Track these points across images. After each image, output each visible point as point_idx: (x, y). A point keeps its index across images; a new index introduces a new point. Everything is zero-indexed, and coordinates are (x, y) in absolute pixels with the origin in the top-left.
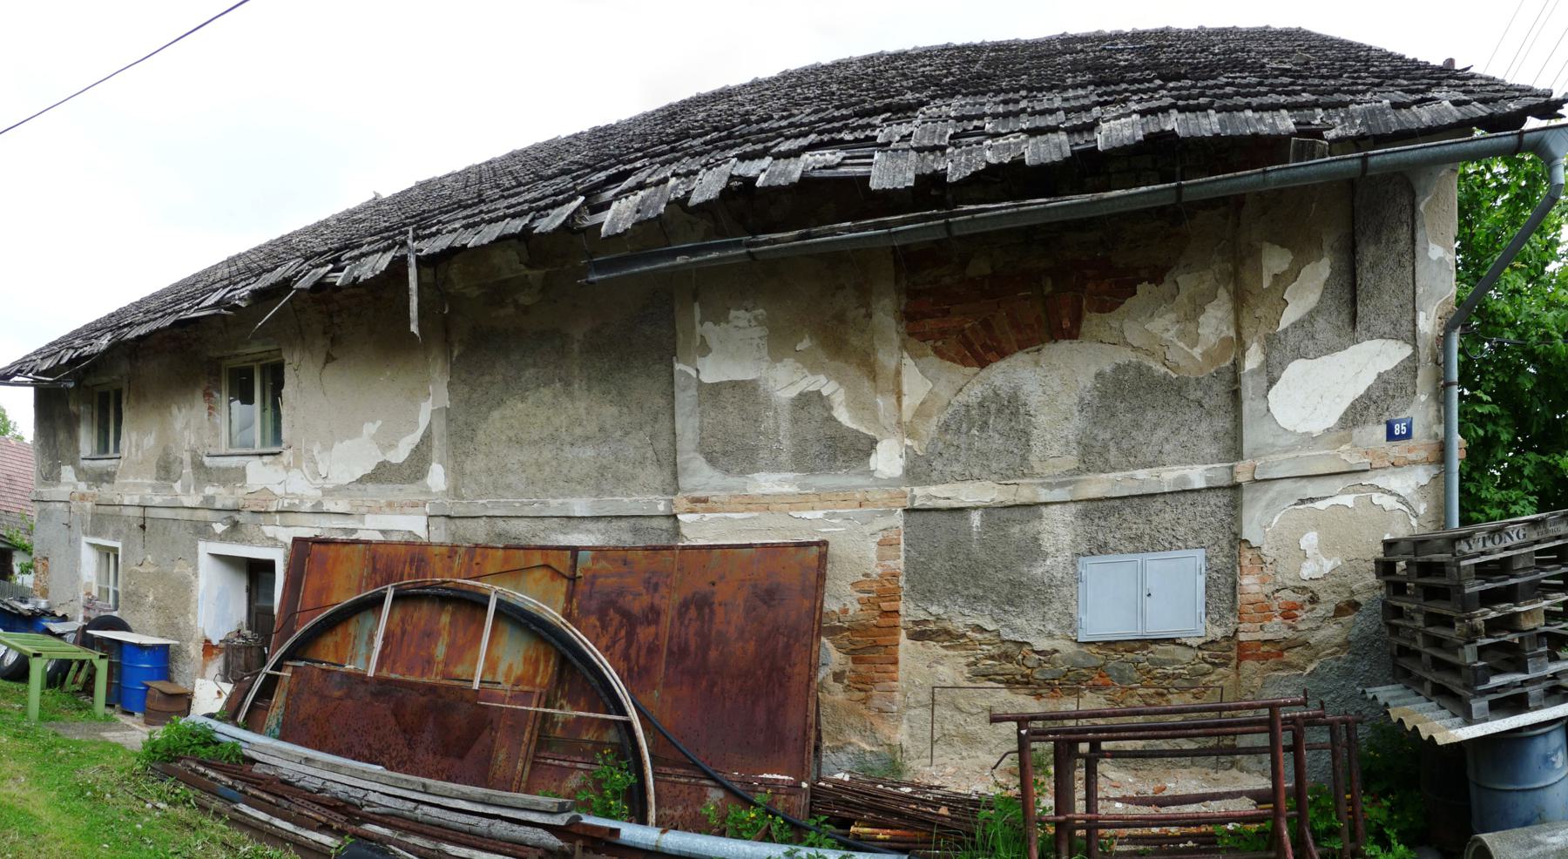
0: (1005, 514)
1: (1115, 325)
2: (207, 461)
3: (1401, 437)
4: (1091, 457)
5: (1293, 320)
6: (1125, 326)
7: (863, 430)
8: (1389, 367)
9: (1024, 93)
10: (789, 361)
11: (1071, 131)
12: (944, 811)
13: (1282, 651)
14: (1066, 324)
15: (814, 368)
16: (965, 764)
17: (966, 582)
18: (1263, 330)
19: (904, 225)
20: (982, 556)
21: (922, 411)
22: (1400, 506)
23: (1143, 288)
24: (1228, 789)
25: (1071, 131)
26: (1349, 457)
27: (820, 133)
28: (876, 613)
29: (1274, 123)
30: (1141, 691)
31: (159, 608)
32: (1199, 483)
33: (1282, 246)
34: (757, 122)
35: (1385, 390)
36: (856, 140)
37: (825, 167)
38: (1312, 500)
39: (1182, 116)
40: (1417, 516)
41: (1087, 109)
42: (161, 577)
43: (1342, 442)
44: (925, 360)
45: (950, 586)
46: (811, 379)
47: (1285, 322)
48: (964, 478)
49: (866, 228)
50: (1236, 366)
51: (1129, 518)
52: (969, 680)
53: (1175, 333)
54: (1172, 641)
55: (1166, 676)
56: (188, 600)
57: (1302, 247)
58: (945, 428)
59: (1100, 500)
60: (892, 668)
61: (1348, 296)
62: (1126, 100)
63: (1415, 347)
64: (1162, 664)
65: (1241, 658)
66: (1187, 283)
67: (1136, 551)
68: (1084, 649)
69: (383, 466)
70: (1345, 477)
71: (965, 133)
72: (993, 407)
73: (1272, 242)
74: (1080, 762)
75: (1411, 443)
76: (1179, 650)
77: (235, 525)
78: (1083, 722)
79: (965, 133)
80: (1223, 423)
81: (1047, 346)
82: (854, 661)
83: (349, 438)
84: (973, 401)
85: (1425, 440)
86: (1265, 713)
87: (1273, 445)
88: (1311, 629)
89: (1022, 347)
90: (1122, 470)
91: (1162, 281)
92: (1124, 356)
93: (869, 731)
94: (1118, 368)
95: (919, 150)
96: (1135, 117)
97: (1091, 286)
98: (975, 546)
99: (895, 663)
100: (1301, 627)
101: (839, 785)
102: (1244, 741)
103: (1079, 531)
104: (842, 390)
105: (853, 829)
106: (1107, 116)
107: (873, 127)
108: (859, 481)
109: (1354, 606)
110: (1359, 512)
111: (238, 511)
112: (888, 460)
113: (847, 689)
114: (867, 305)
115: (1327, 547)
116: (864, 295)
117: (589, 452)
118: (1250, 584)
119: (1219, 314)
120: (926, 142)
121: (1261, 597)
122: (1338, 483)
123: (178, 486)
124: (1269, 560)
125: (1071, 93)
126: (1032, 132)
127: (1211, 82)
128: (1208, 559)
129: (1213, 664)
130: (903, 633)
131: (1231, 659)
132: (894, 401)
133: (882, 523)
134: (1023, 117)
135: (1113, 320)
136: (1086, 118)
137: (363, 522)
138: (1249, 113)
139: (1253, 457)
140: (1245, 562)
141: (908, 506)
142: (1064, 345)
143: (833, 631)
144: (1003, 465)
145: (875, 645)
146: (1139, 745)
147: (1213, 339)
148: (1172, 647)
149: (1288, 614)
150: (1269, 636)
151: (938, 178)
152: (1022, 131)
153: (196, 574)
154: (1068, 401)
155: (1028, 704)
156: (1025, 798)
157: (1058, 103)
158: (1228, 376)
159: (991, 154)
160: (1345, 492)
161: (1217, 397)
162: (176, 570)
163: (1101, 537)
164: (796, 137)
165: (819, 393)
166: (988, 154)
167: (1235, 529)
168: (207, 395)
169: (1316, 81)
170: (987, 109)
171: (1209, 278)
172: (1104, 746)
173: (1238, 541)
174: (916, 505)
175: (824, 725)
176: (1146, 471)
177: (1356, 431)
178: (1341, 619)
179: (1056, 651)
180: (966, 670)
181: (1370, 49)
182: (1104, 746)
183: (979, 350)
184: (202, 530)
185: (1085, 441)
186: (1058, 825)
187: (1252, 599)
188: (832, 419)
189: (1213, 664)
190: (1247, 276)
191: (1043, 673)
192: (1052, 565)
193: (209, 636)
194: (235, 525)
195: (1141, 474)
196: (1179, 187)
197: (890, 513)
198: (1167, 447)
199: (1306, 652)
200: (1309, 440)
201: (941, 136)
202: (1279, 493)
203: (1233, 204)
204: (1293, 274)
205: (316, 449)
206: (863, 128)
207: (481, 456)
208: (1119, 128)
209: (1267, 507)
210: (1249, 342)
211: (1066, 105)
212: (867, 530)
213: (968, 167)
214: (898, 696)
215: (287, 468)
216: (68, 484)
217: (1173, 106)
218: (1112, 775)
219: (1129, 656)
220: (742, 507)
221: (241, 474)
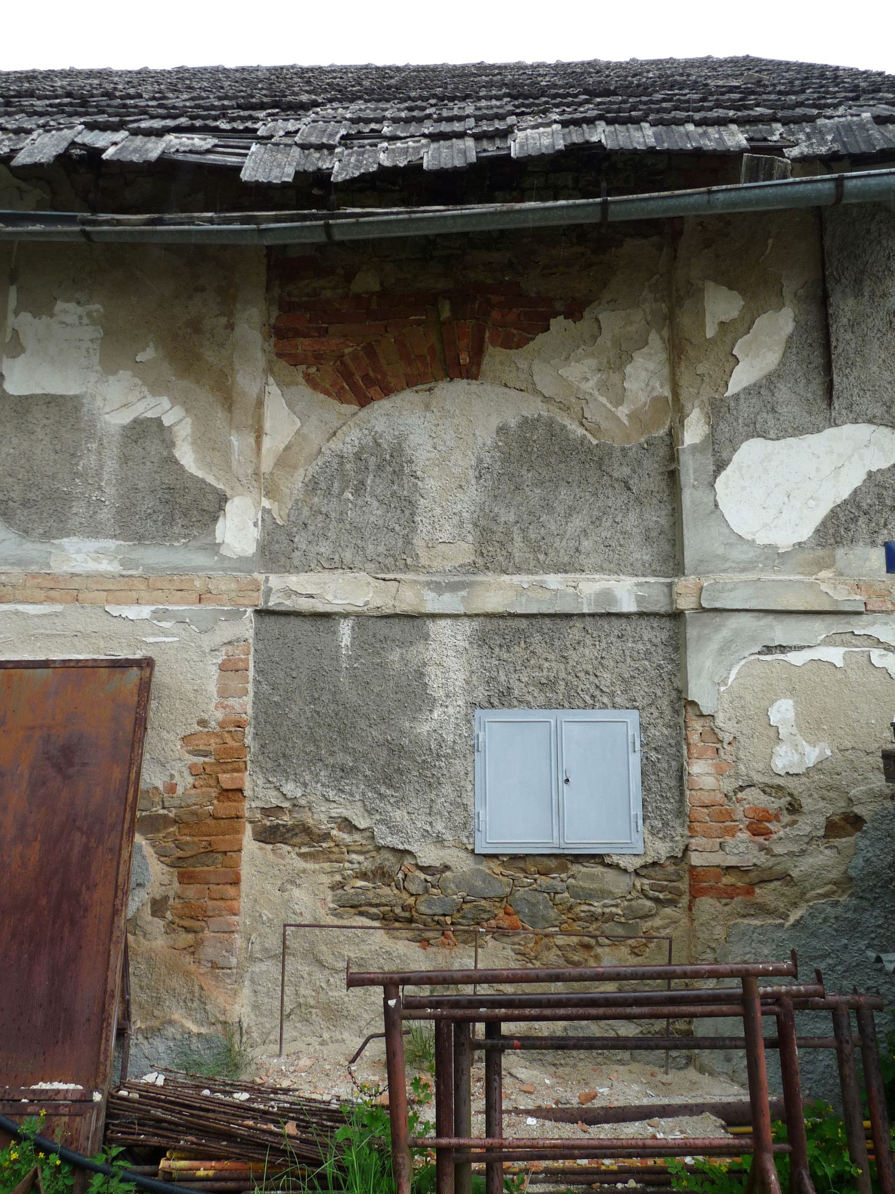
0: (382, 628)
1: (523, 365)
4: (492, 549)
5: (745, 383)
6: (535, 369)
7: (211, 480)
9: (433, 101)
10: (125, 375)
11: (478, 137)
12: (291, 1128)
13: (752, 885)
14: (464, 359)
15: (156, 388)
16: (319, 1057)
17: (332, 742)
18: (707, 392)
19: (275, 223)
20: (353, 697)
21: (284, 461)
23: (558, 324)
24: (679, 1104)
25: (478, 137)
26: (831, 590)
27: (192, 118)
28: (214, 792)
29: (721, 138)
30: (561, 940)
32: (628, 606)
33: (731, 288)
34: (121, 98)
35: (880, 497)
36: (234, 130)
37: (191, 152)
38: (782, 649)
39: (611, 128)
41: (502, 117)
43: (821, 565)
44: (293, 389)
45: (311, 748)
46: (151, 400)
48: (335, 565)
49: (229, 221)
50: (673, 438)
51: (539, 651)
52: (334, 913)
53: (595, 381)
55: (593, 917)
57: (757, 288)
58: (312, 486)
59: (501, 616)
60: (231, 891)
61: (818, 361)
62: (545, 112)
64: (587, 896)
65: (696, 892)
66: (612, 321)
67: (548, 706)
68: (484, 867)
70: (829, 619)
71: (360, 135)
72: (372, 461)
74: (480, 1054)
76: (610, 874)
78: (484, 990)
79: (360, 135)
80: (657, 517)
81: (441, 384)
82: (185, 878)
84: (349, 450)
86: (733, 985)
87: (725, 559)
88: (791, 854)
89: (411, 383)
90: (529, 572)
91: (581, 317)
92: (534, 408)
93: (197, 1001)
94: (525, 422)
95: (304, 147)
96: (555, 127)
97: (495, 314)
98: (344, 680)
99: (236, 882)
100: (778, 849)
101: (149, 1094)
102: (704, 1028)
103: (476, 664)
104: (189, 420)
105: (163, 1163)
106: (524, 125)
107: (256, 120)
108: (200, 559)
109: (854, 822)
112: (238, 530)
113: (170, 928)
114: (230, 314)
115: (810, 725)
116: (228, 300)
118: (700, 770)
119: (651, 366)
120: (313, 140)
121: (719, 797)
122: (819, 628)
124: (727, 738)
125: (483, 103)
126: (434, 137)
127: (644, 99)
128: (643, 728)
129: (656, 900)
130: (248, 827)
131: (680, 894)
132: (252, 441)
133: (226, 631)
134: (427, 123)
135: (521, 358)
136: (499, 125)
138: (691, 127)
139: (699, 574)
140: (694, 738)
142: (461, 385)
143: (154, 824)
144: (381, 549)
145: (210, 851)
146: (557, 1028)
147: (643, 398)
148: (599, 870)
149: (759, 827)
150: (732, 861)
151: (322, 177)
152: (424, 135)
154: (463, 462)
155: (408, 955)
156: (394, 1109)
157: (470, 109)
158: (663, 451)
159: (384, 157)
160: (829, 641)
161: (649, 480)
163: (502, 678)
164: (164, 118)
165: (158, 421)
166: (382, 156)
167: (677, 683)
169: (773, 97)
170: (388, 114)
171: (638, 317)
172: (506, 1028)
173: (682, 704)
174: (272, 604)
175: (136, 994)
176: (560, 576)
177: (840, 552)
178: (836, 842)
179: (447, 868)
180: (329, 896)
181: (837, 69)
182: (506, 1028)
183: (360, 383)
185: (482, 522)
186: (442, 1151)
187: (706, 799)
188: (172, 460)
189: (656, 900)
190: (686, 320)
191: (430, 903)
192: (438, 722)
195: (554, 580)
196: (605, 204)
197: (235, 615)
198: (586, 544)
199: (786, 890)
200: (772, 556)
201: (332, 135)
202: (736, 632)
203: (666, 230)
206: (244, 119)
208: (535, 138)
209: (721, 651)
210: (688, 406)
211: (478, 113)
212: (207, 642)
213: (357, 167)
214: (239, 941)
217: (600, 117)
218: (523, 1073)
219: (543, 880)
220: (42, 594)
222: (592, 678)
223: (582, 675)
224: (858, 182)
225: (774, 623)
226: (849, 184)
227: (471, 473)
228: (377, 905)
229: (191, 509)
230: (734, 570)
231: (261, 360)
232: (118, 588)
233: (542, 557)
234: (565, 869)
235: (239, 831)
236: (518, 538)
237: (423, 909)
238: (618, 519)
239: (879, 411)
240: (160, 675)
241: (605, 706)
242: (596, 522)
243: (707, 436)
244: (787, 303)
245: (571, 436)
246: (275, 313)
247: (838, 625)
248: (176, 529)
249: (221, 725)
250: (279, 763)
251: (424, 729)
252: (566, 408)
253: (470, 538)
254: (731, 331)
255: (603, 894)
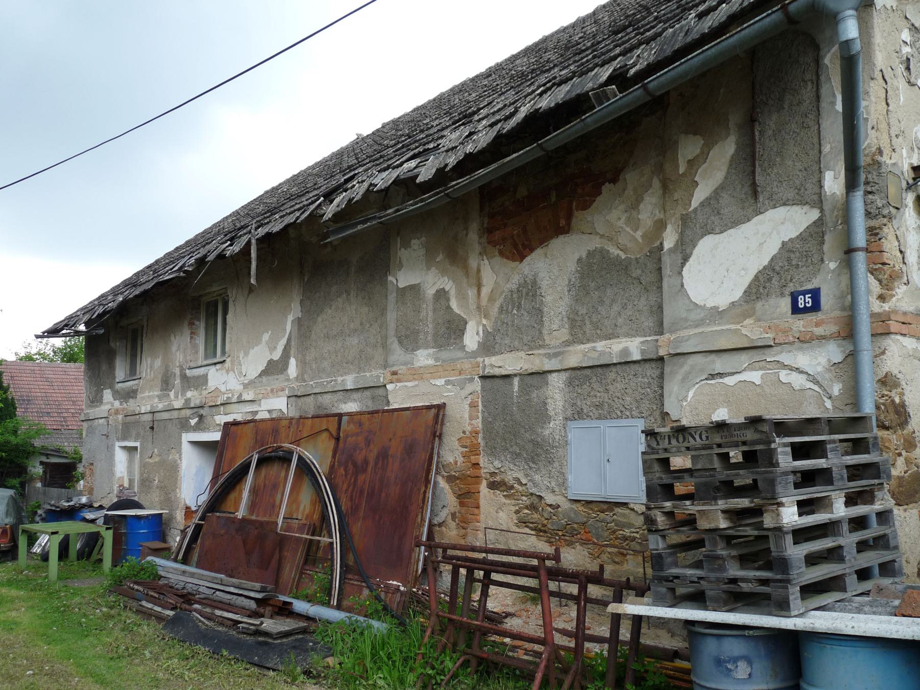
0: (529, 380)
2: (188, 373)
3: (806, 310)
7: (462, 315)
8: (794, 234)
15: (443, 272)
22: (810, 385)
26: (751, 331)
31: (162, 488)
32: (637, 356)
33: (695, 134)
35: (789, 260)
38: (721, 375)
40: (830, 398)
42: (162, 463)
43: (746, 315)
47: (695, 203)
51: (595, 387)
53: (616, 224)
54: (625, 504)
55: (625, 538)
56: (177, 479)
57: (707, 127)
60: (476, 511)
63: (822, 211)
64: (622, 526)
66: (631, 178)
68: (574, 506)
69: (270, 362)
73: (687, 133)
75: (819, 316)
77: (201, 417)
82: (462, 504)
83: (257, 345)
84: (514, 287)
85: (837, 313)
87: (686, 320)
92: (595, 243)
97: (579, 191)
99: (478, 507)
110: (767, 390)
111: (202, 407)
112: (471, 339)
117: (354, 341)
119: (654, 200)
122: (744, 359)
123: (172, 394)
130: (484, 483)
137: (260, 405)
141: (481, 374)
144: (529, 338)
148: (627, 512)
153: (180, 459)
162: (171, 457)
163: (579, 403)
168: (191, 324)
172: (495, 576)
177: (759, 305)
179: (559, 506)
180: (515, 517)
183: (519, 250)
184: (184, 425)
188: (449, 307)
191: (553, 524)
192: (552, 428)
193: (189, 503)
194: (201, 417)
196: (538, 145)
197: (471, 380)
200: (716, 314)
204: (703, 156)
205: (241, 355)
207: (313, 350)
209: (684, 380)
215: (228, 372)
216: (108, 403)
220: (411, 377)
221: (204, 378)
222: (620, 401)
223: (616, 399)
224: (655, 83)
225: (716, 358)
226: (651, 86)
227: (566, 289)
228: (532, 523)
229: (453, 329)
230: (691, 327)
231: (477, 248)
232: (433, 372)
233: (599, 332)
234: (612, 510)
235: (479, 483)
236: (588, 322)
237: (549, 526)
238: (635, 303)
239: (791, 194)
240: (449, 411)
241: (627, 417)
242: (624, 307)
243: (677, 241)
244: (732, 132)
245: (611, 256)
246: (486, 220)
247: (756, 356)
248: (452, 341)
249: (471, 433)
250: (492, 451)
251: (547, 432)
252: (610, 239)
253: (567, 326)
254: (693, 164)
255: (630, 525)
